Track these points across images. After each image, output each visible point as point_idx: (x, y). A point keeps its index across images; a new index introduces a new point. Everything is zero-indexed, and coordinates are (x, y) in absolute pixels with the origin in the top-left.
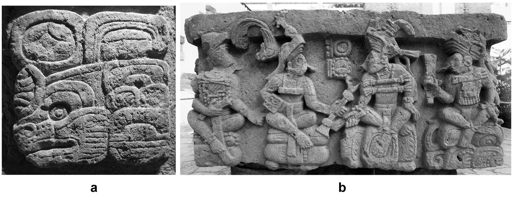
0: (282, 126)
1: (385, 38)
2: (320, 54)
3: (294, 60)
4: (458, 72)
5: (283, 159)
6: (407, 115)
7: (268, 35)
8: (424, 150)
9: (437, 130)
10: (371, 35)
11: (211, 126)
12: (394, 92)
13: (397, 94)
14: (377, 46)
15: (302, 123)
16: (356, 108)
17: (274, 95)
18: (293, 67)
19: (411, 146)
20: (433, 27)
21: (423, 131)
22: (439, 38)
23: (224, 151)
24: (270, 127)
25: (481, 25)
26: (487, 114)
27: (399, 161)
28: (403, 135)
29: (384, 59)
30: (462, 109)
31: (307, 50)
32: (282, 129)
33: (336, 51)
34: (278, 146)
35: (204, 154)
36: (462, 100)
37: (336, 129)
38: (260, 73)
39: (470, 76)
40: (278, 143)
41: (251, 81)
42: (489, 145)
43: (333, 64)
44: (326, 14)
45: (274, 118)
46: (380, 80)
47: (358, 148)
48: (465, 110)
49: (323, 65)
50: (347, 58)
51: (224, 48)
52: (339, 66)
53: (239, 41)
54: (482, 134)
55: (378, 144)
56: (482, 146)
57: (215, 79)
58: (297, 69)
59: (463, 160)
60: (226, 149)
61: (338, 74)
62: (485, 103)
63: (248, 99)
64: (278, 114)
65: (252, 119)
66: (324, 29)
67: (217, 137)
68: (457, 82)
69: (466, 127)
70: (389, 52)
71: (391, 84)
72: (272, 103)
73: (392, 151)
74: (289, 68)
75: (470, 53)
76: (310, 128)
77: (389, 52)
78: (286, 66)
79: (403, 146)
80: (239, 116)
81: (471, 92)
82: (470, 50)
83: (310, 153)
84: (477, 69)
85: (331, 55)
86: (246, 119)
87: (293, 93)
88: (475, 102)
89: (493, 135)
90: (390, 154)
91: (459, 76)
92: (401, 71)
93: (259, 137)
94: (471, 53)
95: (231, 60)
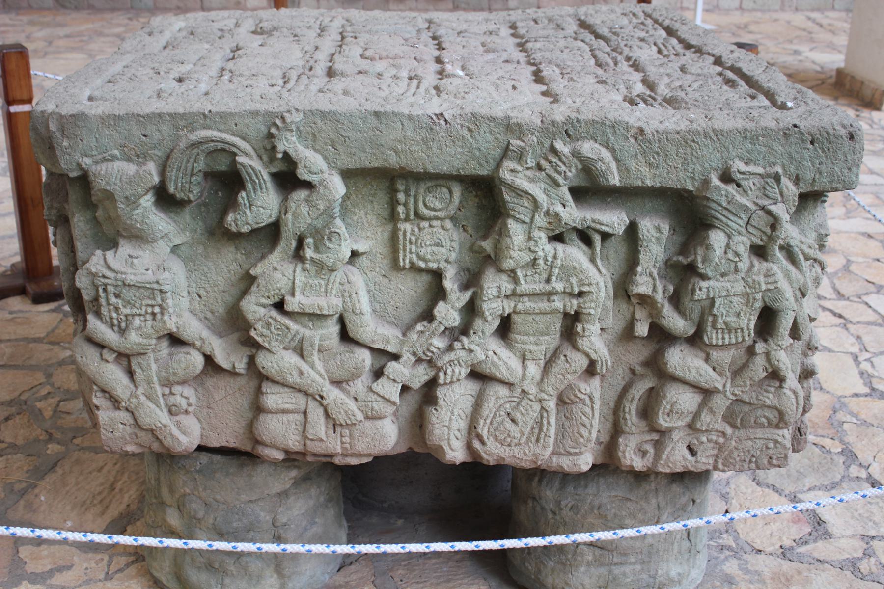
1: (545, 191)
4: (710, 274)
5: (297, 444)
7: (256, 175)
8: (616, 431)
9: (652, 389)
10: (509, 184)
11: (131, 373)
12: (555, 311)
13: (561, 316)
14: (520, 209)
15: (338, 375)
16: (463, 345)
17: (274, 313)
19: (584, 426)
21: (619, 389)
22: (679, 187)
23: (165, 426)
25: (791, 157)
27: (553, 453)
28: (569, 401)
29: (535, 241)
32: (294, 386)
33: (421, 205)
34: (285, 417)
35: (121, 431)
36: (711, 333)
38: (232, 249)
39: (735, 284)
40: (285, 412)
41: (209, 268)
42: (762, 426)
43: (413, 238)
44: (399, 124)
46: (524, 287)
47: (463, 424)
48: (715, 354)
49: (386, 235)
50: (448, 224)
52: (428, 243)
53: (182, 186)
54: (750, 404)
56: (745, 427)
58: (327, 257)
61: (425, 261)
62: (766, 341)
64: (284, 353)
65: (221, 359)
66: (393, 161)
67: (146, 396)
69: (714, 390)
70: (549, 223)
71: (549, 295)
73: (539, 434)
74: (309, 253)
75: (747, 229)
76: (356, 382)
77: (549, 223)
79: (567, 423)
81: (734, 319)
82: (748, 223)
83: (356, 434)
85: (407, 215)
86: (209, 360)
87: (319, 312)
90: (533, 439)
91: (711, 283)
92: (575, 268)
93: (237, 395)
94: (750, 229)
95: (164, 225)
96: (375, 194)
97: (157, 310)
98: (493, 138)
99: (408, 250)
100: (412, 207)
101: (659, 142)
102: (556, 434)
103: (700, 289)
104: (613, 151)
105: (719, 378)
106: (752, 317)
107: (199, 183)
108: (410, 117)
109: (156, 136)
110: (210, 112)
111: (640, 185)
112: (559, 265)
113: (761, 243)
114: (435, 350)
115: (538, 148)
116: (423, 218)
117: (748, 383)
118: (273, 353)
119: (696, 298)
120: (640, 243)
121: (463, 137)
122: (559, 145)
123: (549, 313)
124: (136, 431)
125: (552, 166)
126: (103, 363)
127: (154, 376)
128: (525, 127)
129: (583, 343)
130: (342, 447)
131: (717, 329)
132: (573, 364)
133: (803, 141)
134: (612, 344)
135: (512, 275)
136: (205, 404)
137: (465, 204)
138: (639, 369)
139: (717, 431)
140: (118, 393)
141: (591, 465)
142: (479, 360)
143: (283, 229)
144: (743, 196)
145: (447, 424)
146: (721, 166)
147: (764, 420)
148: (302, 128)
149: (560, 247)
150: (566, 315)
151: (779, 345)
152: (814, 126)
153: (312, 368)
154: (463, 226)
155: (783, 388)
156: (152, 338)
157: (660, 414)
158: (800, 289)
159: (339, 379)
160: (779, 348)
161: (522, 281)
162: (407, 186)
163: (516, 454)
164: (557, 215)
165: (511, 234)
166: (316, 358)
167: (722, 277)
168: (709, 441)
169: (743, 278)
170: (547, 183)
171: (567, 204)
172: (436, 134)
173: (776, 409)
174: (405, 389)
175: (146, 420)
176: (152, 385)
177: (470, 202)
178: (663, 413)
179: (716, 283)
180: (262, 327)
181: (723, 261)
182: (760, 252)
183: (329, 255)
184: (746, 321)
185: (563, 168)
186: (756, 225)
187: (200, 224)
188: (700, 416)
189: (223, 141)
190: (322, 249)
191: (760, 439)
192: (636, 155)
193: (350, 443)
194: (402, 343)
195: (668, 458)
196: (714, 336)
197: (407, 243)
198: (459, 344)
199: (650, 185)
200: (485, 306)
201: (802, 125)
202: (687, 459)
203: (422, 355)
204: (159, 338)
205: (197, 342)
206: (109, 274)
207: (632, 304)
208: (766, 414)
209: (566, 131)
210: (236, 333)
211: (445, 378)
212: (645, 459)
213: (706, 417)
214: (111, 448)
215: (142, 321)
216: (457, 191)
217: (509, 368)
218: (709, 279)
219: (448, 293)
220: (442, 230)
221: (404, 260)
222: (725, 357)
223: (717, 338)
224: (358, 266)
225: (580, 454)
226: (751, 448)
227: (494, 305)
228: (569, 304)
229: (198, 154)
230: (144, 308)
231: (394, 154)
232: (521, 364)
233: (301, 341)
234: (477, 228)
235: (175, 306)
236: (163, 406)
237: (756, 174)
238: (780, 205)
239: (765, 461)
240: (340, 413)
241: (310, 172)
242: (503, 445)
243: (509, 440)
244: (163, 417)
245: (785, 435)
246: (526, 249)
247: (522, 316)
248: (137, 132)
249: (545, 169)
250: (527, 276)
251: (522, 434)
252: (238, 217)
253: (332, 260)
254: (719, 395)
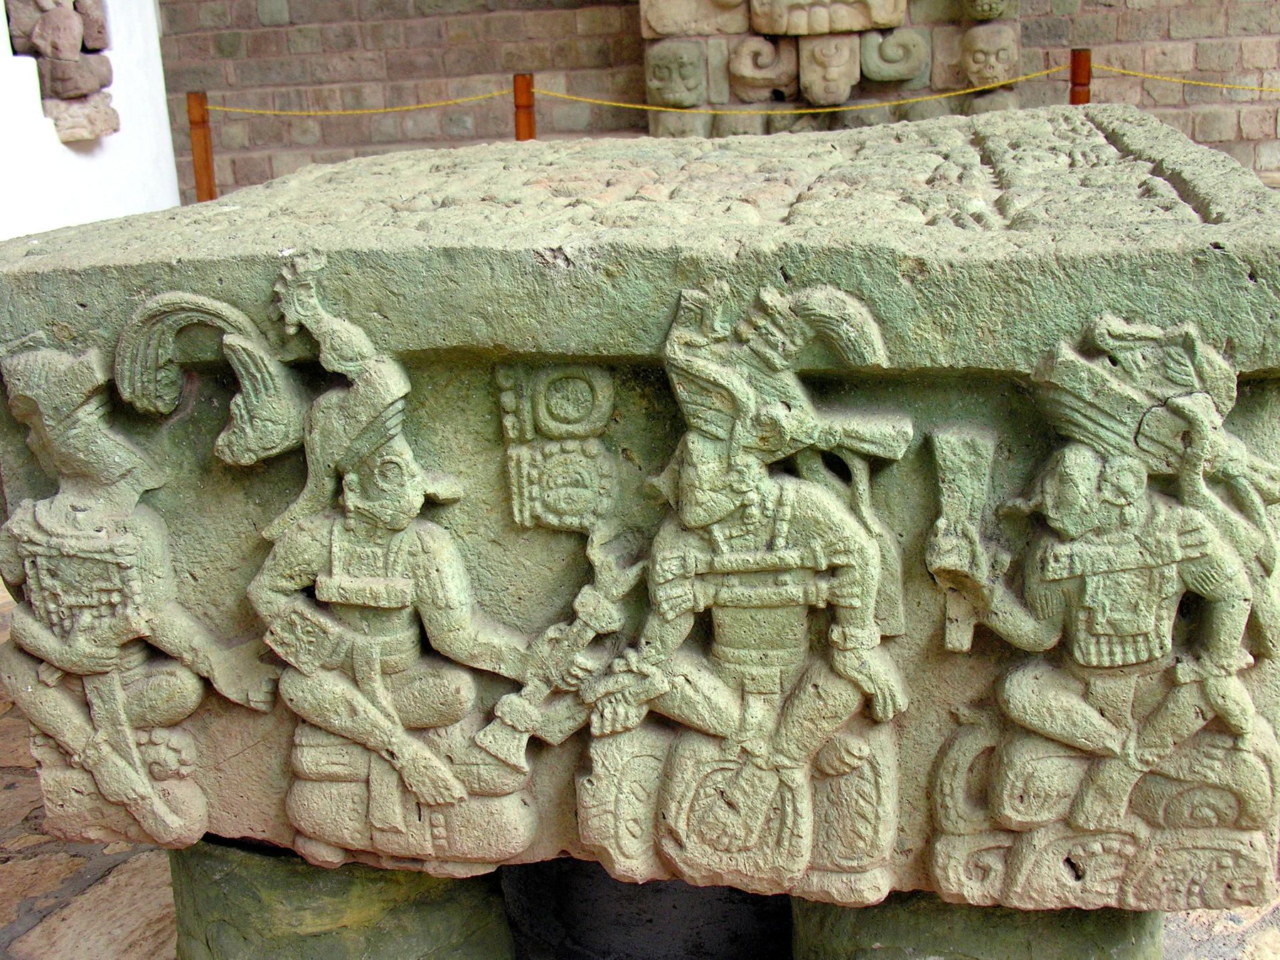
0: (341, 721)
1: (750, 381)
2: (477, 417)
4: (1072, 530)
6: (844, 699)
7: (256, 365)
8: (933, 830)
9: (991, 750)
10: (682, 369)
11: (86, 706)
12: (788, 603)
15: (420, 715)
16: (628, 664)
17: (301, 605)
19: (864, 817)
20: (972, 322)
21: (934, 752)
22: (1002, 367)
23: (143, 798)
24: (298, 720)
26: (1202, 705)
27: (812, 868)
28: (832, 772)
29: (740, 472)
30: (1092, 681)
31: (423, 404)
34: (334, 789)
36: (1087, 644)
37: (555, 736)
38: (240, 496)
39: (1124, 549)
40: (333, 779)
42: (1207, 824)
43: (535, 473)
44: (487, 269)
45: (311, 692)
46: (728, 558)
48: (1100, 686)
49: (493, 468)
50: (594, 446)
51: (94, 418)
52: (560, 481)
53: (144, 388)
54: (1178, 780)
55: (721, 803)
56: (1176, 827)
57: (78, 538)
58: (382, 506)
59: (1088, 878)
60: (150, 789)
61: (558, 513)
63: (205, 599)
64: (323, 675)
65: (223, 685)
66: (482, 334)
67: (112, 746)
68: (1065, 575)
69: (1104, 753)
72: (298, 639)
73: (781, 830)
74: (352, 500)
75: (1137, 444)
76: (450, 729)
77: (763, 439)
78: (339, 491)
79: (833, 813)
80: (179, 673)
81: (1129, 616)
82: (1138, 432)
83: (457, 822)
84: (1163, 510)
85: (522, 431)
86: (207, 683)
87: (372, 603)
88: (1144, 656)
89: (1223, 789)
90: (771, 841)
91: (1077, 547)
92: (817, 522)
93: (262, 749)
94: (1144, 444)
95: (124, 455)
96: (468, 396)
97: (116, 598)
98: (651, 287)
99: (526, 494)
100: (527, 416)
101: (956, 283)
102: (816, 832)
103: (1057, 560)
104: (870, 303)
105: (1113, 731)
107: (173, 383)
108: (505, 256)
109: (100, 305)
110: (179, 261)
111: (929, 364)
112: (788, 517)
113: (1170, 471)
114: (581, 674)
115: (733, 303)
117: (1170, 740)
118: (301, 673)
119: (1050, 575)
120: (941, 475)
121: (598, 287)
122: (771, 296)
123: (777, 607)
124: (100, 805)
125: (760, 335)
126: (40, 687)
127: (122, 712)
128: (707, 265)
129: (846, 662)
130: (434, 846)
132: (830, 702)
133: (1234, 274)
134: (912, 667)
135: (704, 532)
136: (211, 762)
137: (623, 410)
138: (964, 712)
139: (1120, 832)
140: (66, 739)
141: (885, 892)
142: (658, 693)
143: (310, 458)
144: (1124, 381)
145: (612, 808)
146: (1077, 326)
147: (1208, 813)
148: (326, 283)
149: (790, 484)
150: (812, 610)
151: (1223, 667)
152: (1253, 246)
153: (373, 703)
154: (624, 450)
155: (1240, 750)
156: (111, 647)
157: (1006, 798)
158: (1258, 559)
159: (419, 724)
160: (1223, 672)
161: (725, 548)
163: (741, 867)
164: (775, 424)
165: (695, 459)
166: (378, 685)
167: (1098, 535)
168: (1107, 851)
169: (1137, 538)
170: (753, 366)
171: (793, 402)
172: (550, 284)
173: (1231, 790)
174: (536, 745)
175: (112, 787)
176: (119, 728)
177: (632, 408)
178: (1011, 796)
179: (1086, 547)
180: (282, 629)
181: (1095, 505)
183: (384, 501)
184: (1152, 620)
185: (780, 336)
186: (1155, 436)
187: (188, 453)
188: (1083, 802)
189: (199, 310)
191: (1203, 848)
192: (914, 310)
193: (447, 838)
194: (524, 659)
195: (1028, 881)
196: (1093, 649)
197: (525, 481)
198: (622, 662)
199: (946, 365)
200: (661, 594)
201: (1229, 246)
202: (1065, 885)
203: (560, 682)
204: (124, 646)
205: (185, 655)
206: (38, 537)
207: (940, 591)
208: (1212, 801)
210: (251, 642)
211: (602, 727)
212: (987, 883)
213: (1093, 807)
214: (64, 834)
215: (95, 617)
216: (605, 391)
217: (713, 708)
218: (1072, 540)
219: (597, 569)
220: (583, 458)
221: (521, 512)
222: (1123, 690)
223: (1100, 654)
224: (446, 523)
225: (862, 870)
226: (1188, 867)
227: (677, 591)
228: (813, 589)
229: (163, 333)
230: (95, 595)
231: (482, 322)
232: (739, 701)
233: (350, 654)
234: (650, 454)
235: (146, 592)
236: (138, 763)
237: (1146, 339)
238: (1200, 397)
239: (1219, 892)
240: (424, 784)
241: (342, 357)
242: (716, 849)
243: (726, 840)
244: (140, 783)
245: (1255, 842)
246: (724, 488)
247: (730, 612)
248: (69, 298)
249: (748, 341)
250: (731, 537)
251: (749, 831)
252: (233, 438)
253: (391, 512)
254: (1114, 762)
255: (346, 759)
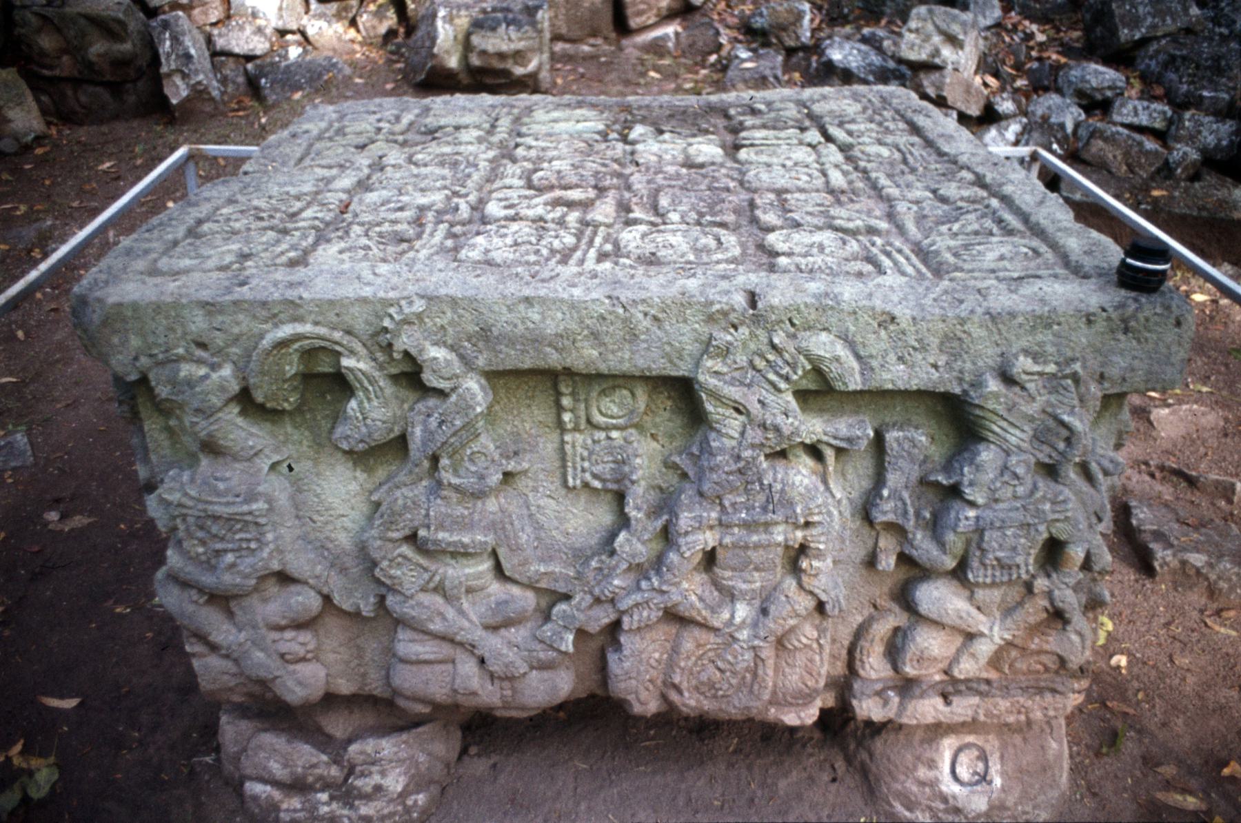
3: (458, 456)
18: (456, 473)
24: (399, 622)
37: (594, 628)
62: (1049, 576)
74: (447, 476)
86: (327, 599)
100: (582, 414)
106: (1032, 551)
116: (597, 427)
131: (984, 565)
137: (653, 407)
150: (787, 547)
162: (574, 389)
182: (1051, 471)
190: (462, 472)
209: (790, 320)
254: (983, 640)
255: (435, 649)
